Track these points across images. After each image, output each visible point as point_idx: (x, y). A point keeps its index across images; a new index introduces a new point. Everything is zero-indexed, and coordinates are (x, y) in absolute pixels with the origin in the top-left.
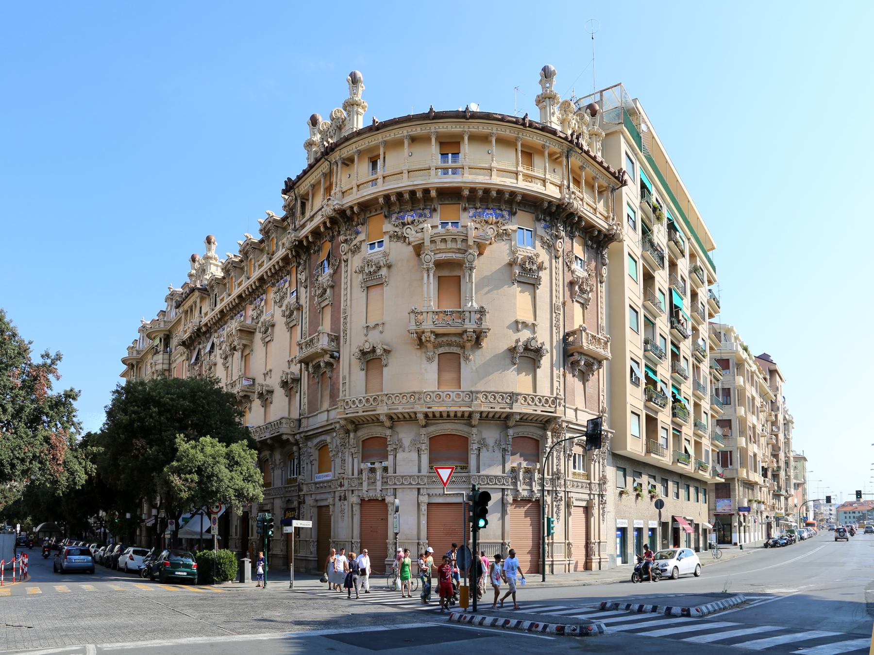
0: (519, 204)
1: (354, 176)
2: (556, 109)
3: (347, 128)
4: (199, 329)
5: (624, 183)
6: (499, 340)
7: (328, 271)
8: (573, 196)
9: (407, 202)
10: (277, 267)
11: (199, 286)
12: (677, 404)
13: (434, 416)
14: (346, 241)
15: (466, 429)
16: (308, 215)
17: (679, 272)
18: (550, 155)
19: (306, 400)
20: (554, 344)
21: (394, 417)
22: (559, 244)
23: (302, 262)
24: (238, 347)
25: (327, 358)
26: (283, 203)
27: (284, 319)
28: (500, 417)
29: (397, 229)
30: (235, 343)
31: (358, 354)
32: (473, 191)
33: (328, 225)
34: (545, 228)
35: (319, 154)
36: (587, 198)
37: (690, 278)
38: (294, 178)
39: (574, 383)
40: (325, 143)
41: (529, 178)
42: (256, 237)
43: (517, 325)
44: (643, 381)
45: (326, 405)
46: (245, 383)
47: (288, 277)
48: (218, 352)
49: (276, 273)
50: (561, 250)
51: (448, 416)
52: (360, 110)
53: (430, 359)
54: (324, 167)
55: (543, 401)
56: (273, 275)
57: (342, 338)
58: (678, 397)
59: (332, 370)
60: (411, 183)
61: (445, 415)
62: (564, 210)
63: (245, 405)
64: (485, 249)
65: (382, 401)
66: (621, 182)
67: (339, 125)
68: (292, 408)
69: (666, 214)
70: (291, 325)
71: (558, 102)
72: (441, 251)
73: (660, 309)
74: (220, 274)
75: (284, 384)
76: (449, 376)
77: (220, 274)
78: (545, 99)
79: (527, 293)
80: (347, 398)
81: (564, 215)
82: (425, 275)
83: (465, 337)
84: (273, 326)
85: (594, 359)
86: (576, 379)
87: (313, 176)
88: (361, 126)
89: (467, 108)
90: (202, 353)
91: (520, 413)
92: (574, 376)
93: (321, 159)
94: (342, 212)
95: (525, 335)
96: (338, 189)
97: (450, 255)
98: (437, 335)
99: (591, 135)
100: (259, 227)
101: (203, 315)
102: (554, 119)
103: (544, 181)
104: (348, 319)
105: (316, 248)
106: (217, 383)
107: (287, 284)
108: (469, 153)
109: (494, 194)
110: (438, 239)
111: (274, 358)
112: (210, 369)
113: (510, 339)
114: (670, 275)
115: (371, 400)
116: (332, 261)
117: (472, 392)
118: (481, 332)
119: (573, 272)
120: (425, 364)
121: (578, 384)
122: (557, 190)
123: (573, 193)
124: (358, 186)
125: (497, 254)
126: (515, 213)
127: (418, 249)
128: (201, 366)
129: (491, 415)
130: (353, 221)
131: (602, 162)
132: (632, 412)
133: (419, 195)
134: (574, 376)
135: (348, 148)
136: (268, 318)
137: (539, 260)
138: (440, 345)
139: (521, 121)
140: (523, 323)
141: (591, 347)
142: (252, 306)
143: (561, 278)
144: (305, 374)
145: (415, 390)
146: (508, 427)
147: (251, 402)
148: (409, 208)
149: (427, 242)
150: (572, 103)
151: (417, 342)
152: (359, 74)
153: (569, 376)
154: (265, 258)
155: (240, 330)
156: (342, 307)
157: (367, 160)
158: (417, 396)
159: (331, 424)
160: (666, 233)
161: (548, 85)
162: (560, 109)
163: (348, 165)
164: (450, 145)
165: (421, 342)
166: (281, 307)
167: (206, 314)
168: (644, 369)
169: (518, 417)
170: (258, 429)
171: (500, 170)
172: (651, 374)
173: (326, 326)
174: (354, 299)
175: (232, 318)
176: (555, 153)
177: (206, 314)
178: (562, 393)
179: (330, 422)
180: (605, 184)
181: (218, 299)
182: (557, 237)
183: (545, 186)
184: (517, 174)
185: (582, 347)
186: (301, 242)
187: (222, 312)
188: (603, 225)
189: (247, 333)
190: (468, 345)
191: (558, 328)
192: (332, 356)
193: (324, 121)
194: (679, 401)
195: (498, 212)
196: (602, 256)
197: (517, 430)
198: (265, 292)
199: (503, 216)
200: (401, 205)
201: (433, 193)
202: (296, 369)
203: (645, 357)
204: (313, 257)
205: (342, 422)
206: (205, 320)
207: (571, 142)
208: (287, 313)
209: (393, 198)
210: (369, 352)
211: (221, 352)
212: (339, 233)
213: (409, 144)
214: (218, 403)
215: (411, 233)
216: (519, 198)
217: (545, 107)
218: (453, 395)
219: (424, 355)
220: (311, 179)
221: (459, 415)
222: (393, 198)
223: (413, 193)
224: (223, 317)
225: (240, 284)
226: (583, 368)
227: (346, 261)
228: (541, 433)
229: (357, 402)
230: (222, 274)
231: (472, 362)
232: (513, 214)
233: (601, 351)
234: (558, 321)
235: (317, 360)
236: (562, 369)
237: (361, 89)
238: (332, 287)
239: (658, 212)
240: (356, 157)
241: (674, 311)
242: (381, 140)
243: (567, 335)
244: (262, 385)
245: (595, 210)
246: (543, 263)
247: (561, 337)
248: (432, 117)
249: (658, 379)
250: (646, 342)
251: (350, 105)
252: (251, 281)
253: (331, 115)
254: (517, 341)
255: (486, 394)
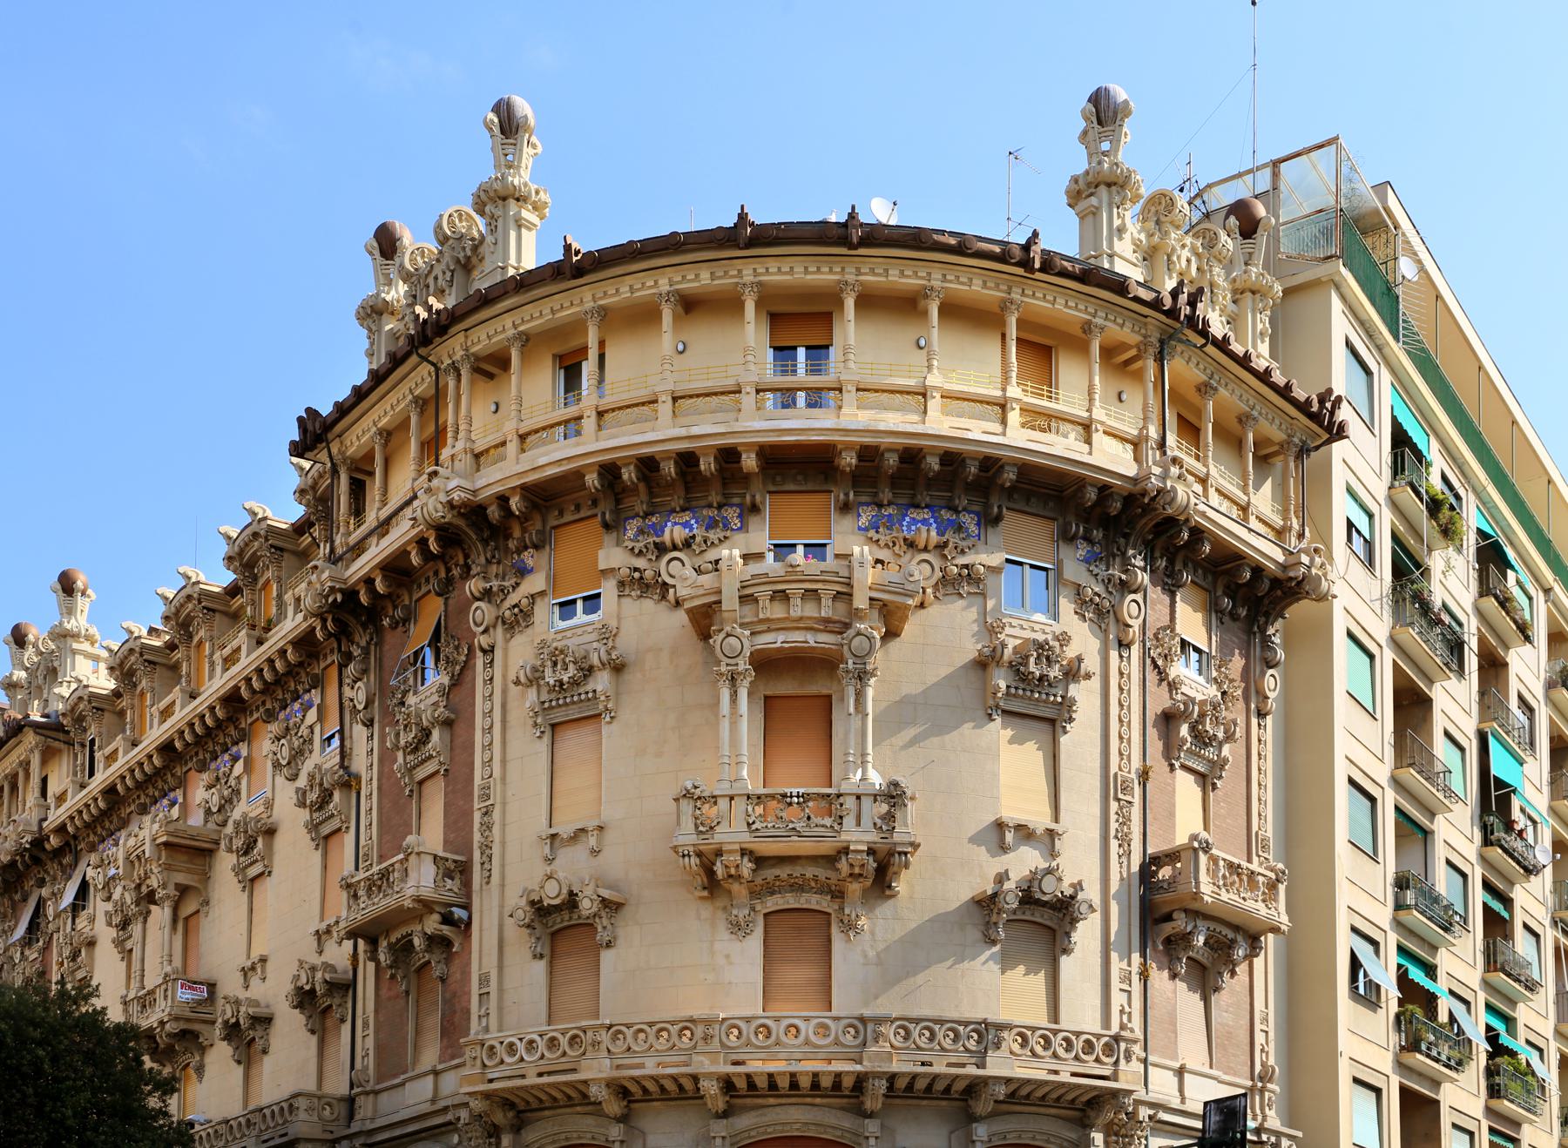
0: (1011, 492)
1: (509, 407)
2: (1129, 217)
3: (487, 266)
4: (39, 842)
5: (1338, 432)
6: (946, 874)
7: (436, 678)
8: (1174, 470)
9: (671, 485)
10: (278, 665)
11: (36, 717)
12: (1503, 1061)
13: (752, 1085)
14: (487, 595)
15: (847, 1122)
16: (372, 517)
17: (1514, 686)
18: (1108, 352)
19: (370, 1042)
20: (1114, 886)
21: (633, 1088)
22: (1130, 607)
23: (356, 652)
24: (160, 893)
25: (432, 924)
26: (295, 481)
27: (305, 815)
28: (948, 1090)
29: (641, 563)
30: (154, 882)
31: (524, 914)
32: (869, 454)
33: (433, 547)
34: (1087, 561)
35: (401, 342)
36: (1218, 473)
37: (1549, 700)
38: (325, 410)
39: (1177, 997)
40: (419, 309)
41: (1041, 419)
42: (218, 578)
43: (1001, 835)
44: (1391, 993)
45: (430, 1056)
46: (184, 995)
47: (315, 696)
48: (99, 906)
49: (279, 681)
50: (1136, 624)
51: (794, 1085)
52: (527, 214)
53: (739, 929)
54: (418, 379)
55: (1079, 1045)
56: (268, 689)
57: (476, 868)
58: (1505, 1039)
59: (448, 960)
60: (683, 432)
61: (784, 1083)
62: (1148, 509)
63: (183, 1059)
64: (904, 619)
65: (596, 1044)
66: (1329, 429)
67: (463, 256)
68: (329, 1066)
69: (1472, 518)
70: (326, 829)
71: (1137, 197)
72: (771, 625)
73: (1448, 791)
74: (104, 683)
75: (304, 999)
76: (798, 974)
77: (104, 683)
78: (1096, 189)
79: (1031, 746)
80: (492, 1037)
81: (1146, 523)
82: (725, 694)
83: (843, 865)
84: (270, 832)
85: (1236, 928)
86: (1181, 986)
87: (386, 405)
88: (530, 262)
89: (852, 215)
90: (50, 912)
91: (1008, 1081)
92: (1174, 976)
93: (407, 355)
94: (473, 512)
95: (1024, 862)
96: (460, 445)
97: (798, 636)
98: (760, 861)
99: (1238, 294)
100: (223, 549)
101: (51, 800)
102: (1124, 247)
103: (1087, 428)
104: (496, 815)
105: (399, 613)
106: (86, 998)
107: (312, 716)
108: (860, 347)
109: (934, 463)
110: (763, 592)
111: (276, 923)
112: (75, 956)
113: (978, 873)
114: (1482, 693)
115: (564, 1041)
116: (446, 650)
117: (863, 1020)
118: (891, 854)
119: (1173, 686)
120: (725, 942)
121: (1187, 1001)
122: (1127, 452)
123: (1175, 460)
124: (523, 438)
125: (944, 635)
126: (997, 520)
127: (704, 619)
128: (46, 949)
129: (921, 1085)
130: (508, 536)
131: (1268, 372)
132: (1356, 1081)
133: (707, 465)
134: (1174, 976)
135: (490, 328)
136: (256, 810)
137: (1071, 652)
138: (771, 889)
139: (1017, 253)
140: (1019, 828)
141: (1225, 896)
142: (206, 777)
143: (1137, 702)
144: (367, 971)
145: (696, 1013)
146: (973, 1118)
147: (203, 1050)
148: (677, 502)
149: (730, 601)
150: (1182, 201)
151: (702, 879)
152: (523, 107)
153: (1159, 978)
154: (242, 637)
155: (166, 844)
156: (477, 781)
157: (549, 362)
158: (699, 1031)
159: (445, 1109)
160: (1474, 575)
161: (1105, 146)
162: (1144, 217)
163: (491, 376)
164: (800, 324)
165: (710, 878)
166: (293, 778)
167: (61, 799)
168: (1394, 959)
169: (1001, 1091)
170: (222, 1129)
171: (950, 390)
172: (1416, 974)
173: (431, 834)
174: (518, 773)
175: (144, 810)
176: (1123, 347)
177: (61, 799)
178: (1136, 1023)
179: (441, 1104)
180: (1278, 436)
181: (97, 755)
182: (1125, 587)
183: (1088, 441)
184: (1003, 406)
185: (1197, 896)
186: (350, 594)
187: (110, 791)
188: (1269, 552)
189: (191, 853)
190: (854, 888)
191: (1125, 840)
192: (447, 919)
193: (416, 242)
194: (1513, 1054)
195: (946, 515)
196: (1266, 642)
197: (1000, 1126)
198: (245, 736)
199: (959, 528)
200: (651, 494)
201: (750, 462)
202: (339, 954)
203: (1398, 924)
204: (391, 638)
205: (477, 1105)
206: (56, 816)
207: (1173, 313)
208: (313, 796)
209: (629, 474)
210: (557, 908)
211: (109, 907)
212: (467, 574)
213: (676, 318)
214: (89, 1057)
215: (682, 575)
216: (1010, 475)
217: (1095, 213)
218: (807, 1029)
219: (721, 915)
220: (381, 414)
221: (826, 1082)
222: (629, 474)
223: (687, 460)
224: (114, 809)
225: (166, 713)
226: (1203, 956)
227: (489, 651)
228: (1073, 1135)
229: (521, 1047)
230: (112, 685)
231: (866, 936)
232: (990, 520)
233: (1261, 909)
234: (1125, 821)
235: (403, 931)
236: (1136, 958)
237: (529, 155)
238: (448, 724)
239: (1445, 513)
240: (515, 355)
241: (1495, 800)
242: (589, 305)
243: (1151, 864)
244: (237, 1002)
245: (1244, 509)
246: (1080, 659)
247: (1135, 868)
248: (744, 238)
249: (1440, 988)
250: (1402, 883)
251: (497, 200)
252: (201, 704)
253: (439, 227)
254: (1001, 878)
255: (906, 1025)
